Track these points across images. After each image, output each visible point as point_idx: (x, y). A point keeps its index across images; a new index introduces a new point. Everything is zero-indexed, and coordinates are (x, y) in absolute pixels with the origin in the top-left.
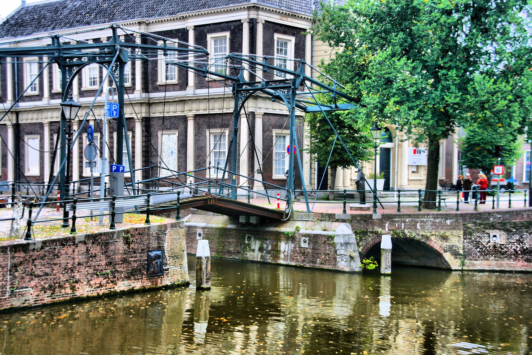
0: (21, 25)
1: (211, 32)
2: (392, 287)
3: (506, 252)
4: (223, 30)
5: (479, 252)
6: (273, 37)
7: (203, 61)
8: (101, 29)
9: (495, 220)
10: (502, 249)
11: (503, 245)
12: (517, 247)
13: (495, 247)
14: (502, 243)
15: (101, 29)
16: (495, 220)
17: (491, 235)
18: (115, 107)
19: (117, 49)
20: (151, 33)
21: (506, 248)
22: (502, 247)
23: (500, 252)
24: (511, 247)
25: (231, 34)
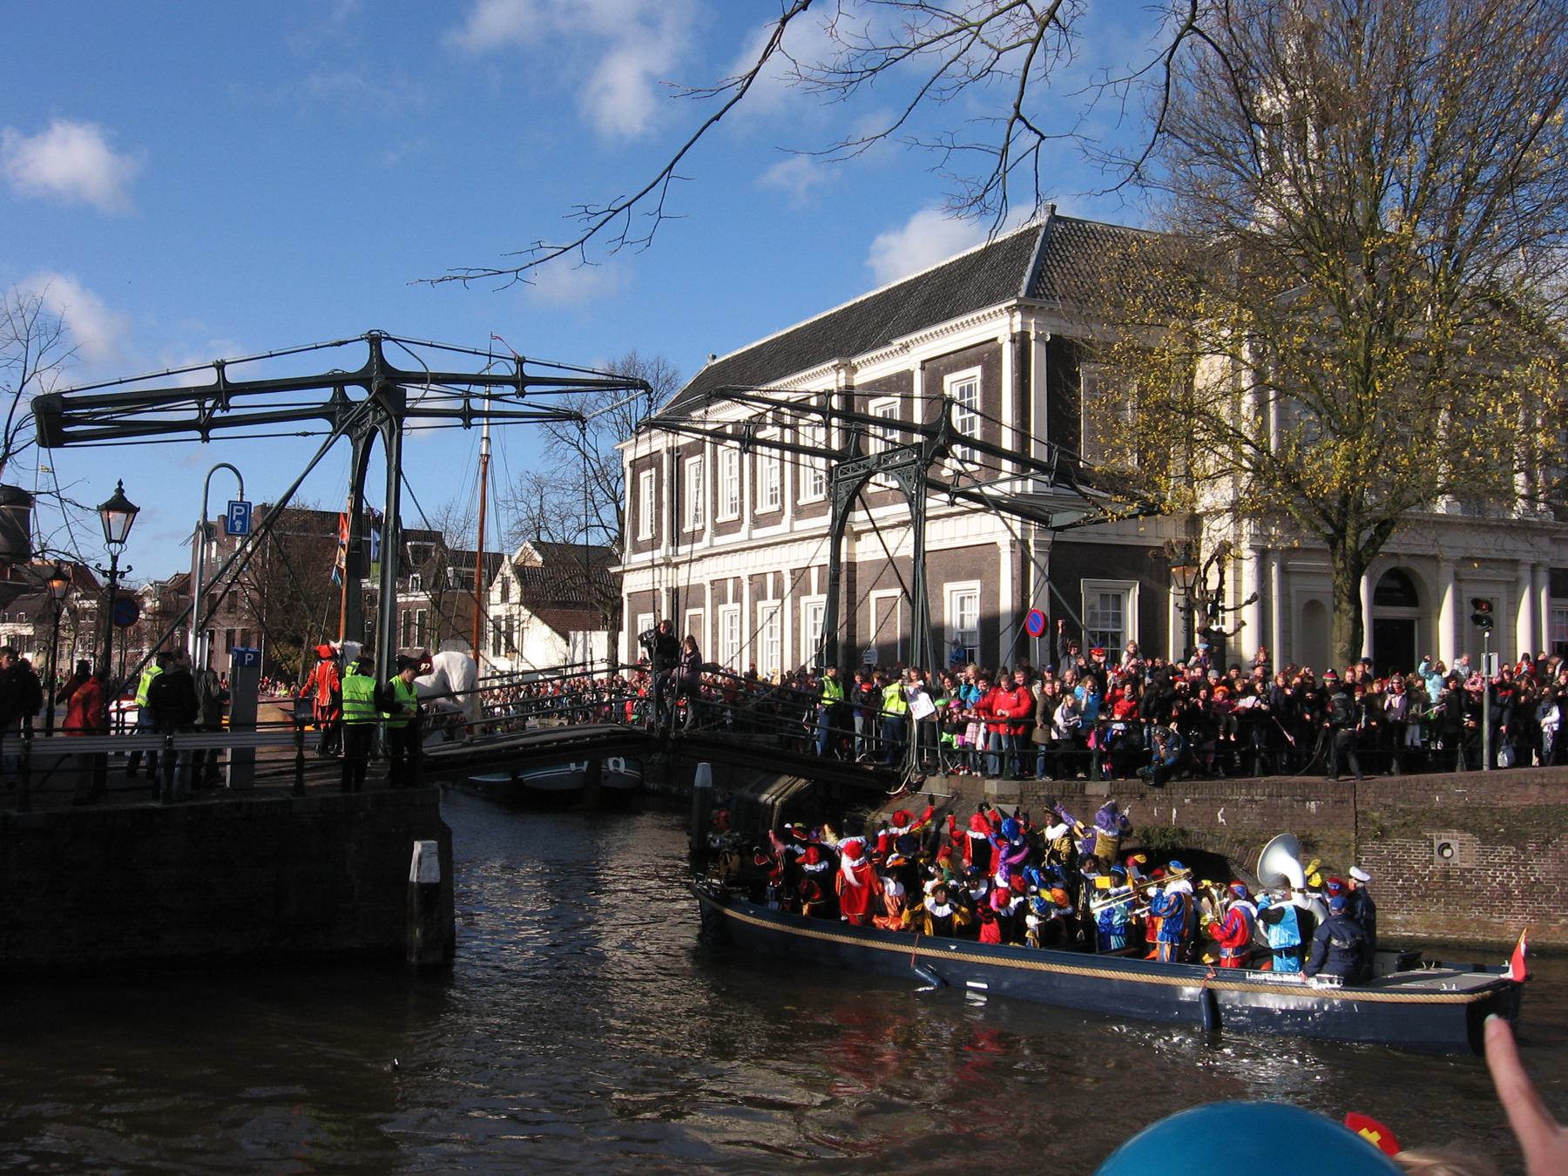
0: (1221, 154)
1: (951, 372)
2: (547, 624)
3: (1478, 890)
4: (969, 364)
5: (1402, 888)
6: (975, 364)
7: (351, 415)
8: (306, 434)
9: (1449, 801)
10: (1469, 882)
11: (1470, 871)
12: (1509, 876)
13: (1447, 876)
14: (1466, 865)
15: (306, 434)
16: (1449, 801)
17: (1437, 843)
18: (238, 511)
19: (1058, 915)
20: (668, 407)
21: (1478, 878)
22: (1469, 876)
23: (1462, 891)
24: (1494, 878)
25: (984, 372)
